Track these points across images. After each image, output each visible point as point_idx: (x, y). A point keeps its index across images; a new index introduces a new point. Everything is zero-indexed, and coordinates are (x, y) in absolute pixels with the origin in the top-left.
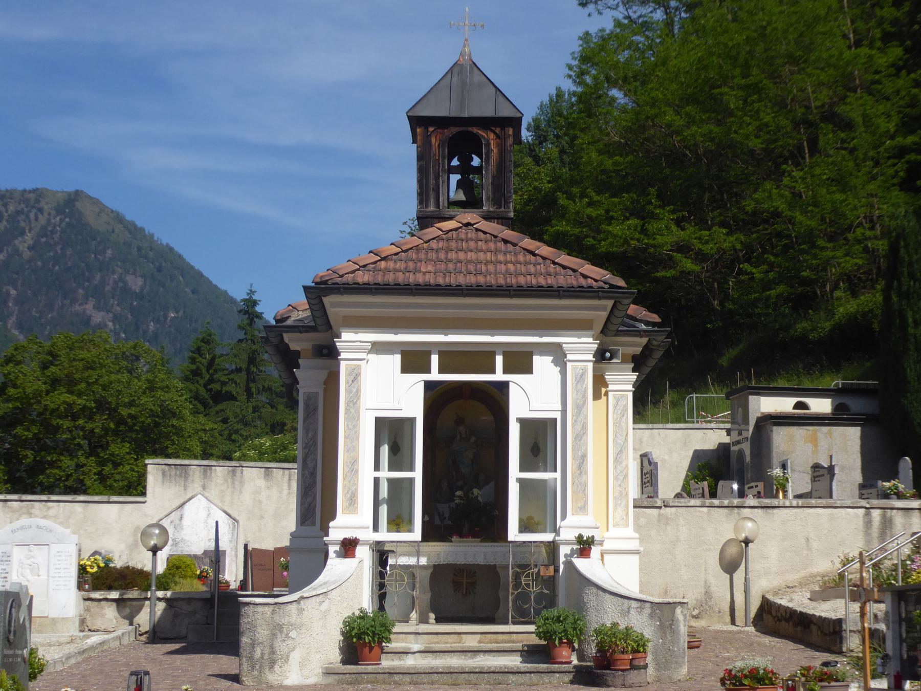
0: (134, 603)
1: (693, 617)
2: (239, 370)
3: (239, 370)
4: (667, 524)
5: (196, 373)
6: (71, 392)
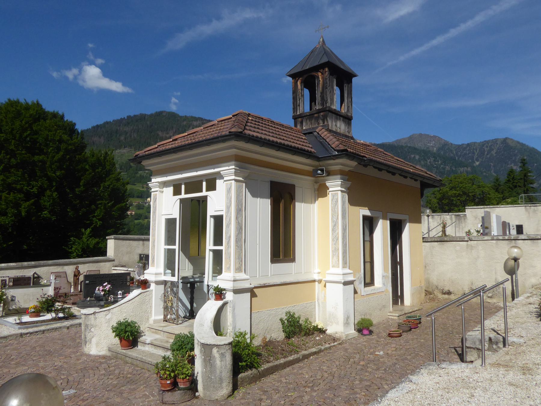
1: (489, 297)
2: (521, 179)
3: (521, 179)
4: (472, 249)
5: (509, 181)
6: (455, 190)
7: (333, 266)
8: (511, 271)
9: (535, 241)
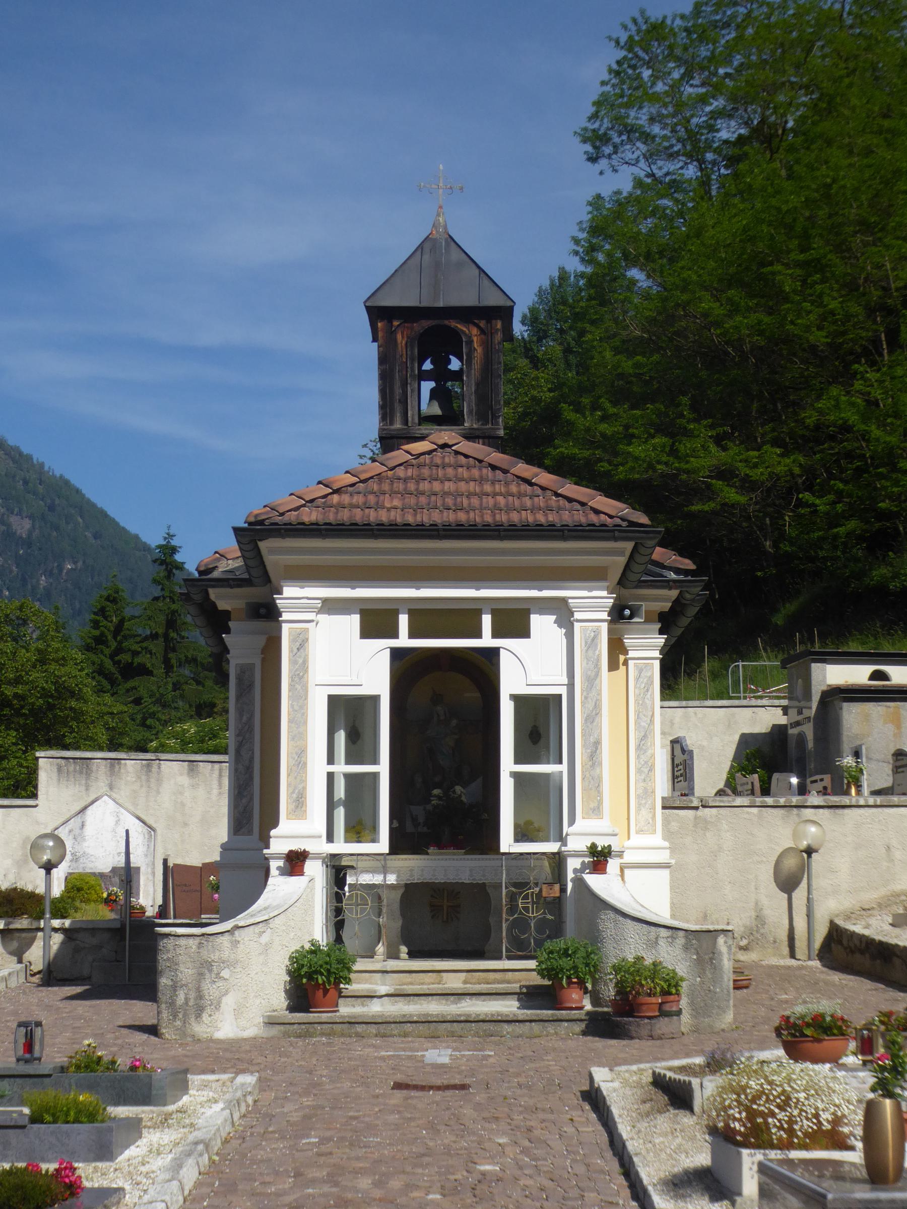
0: (24, 935)
1: (741, 948)
4: (706, 829)
5: (100, 640)
7: (640, 831)
8: (787, 883)
9: (840, 811)
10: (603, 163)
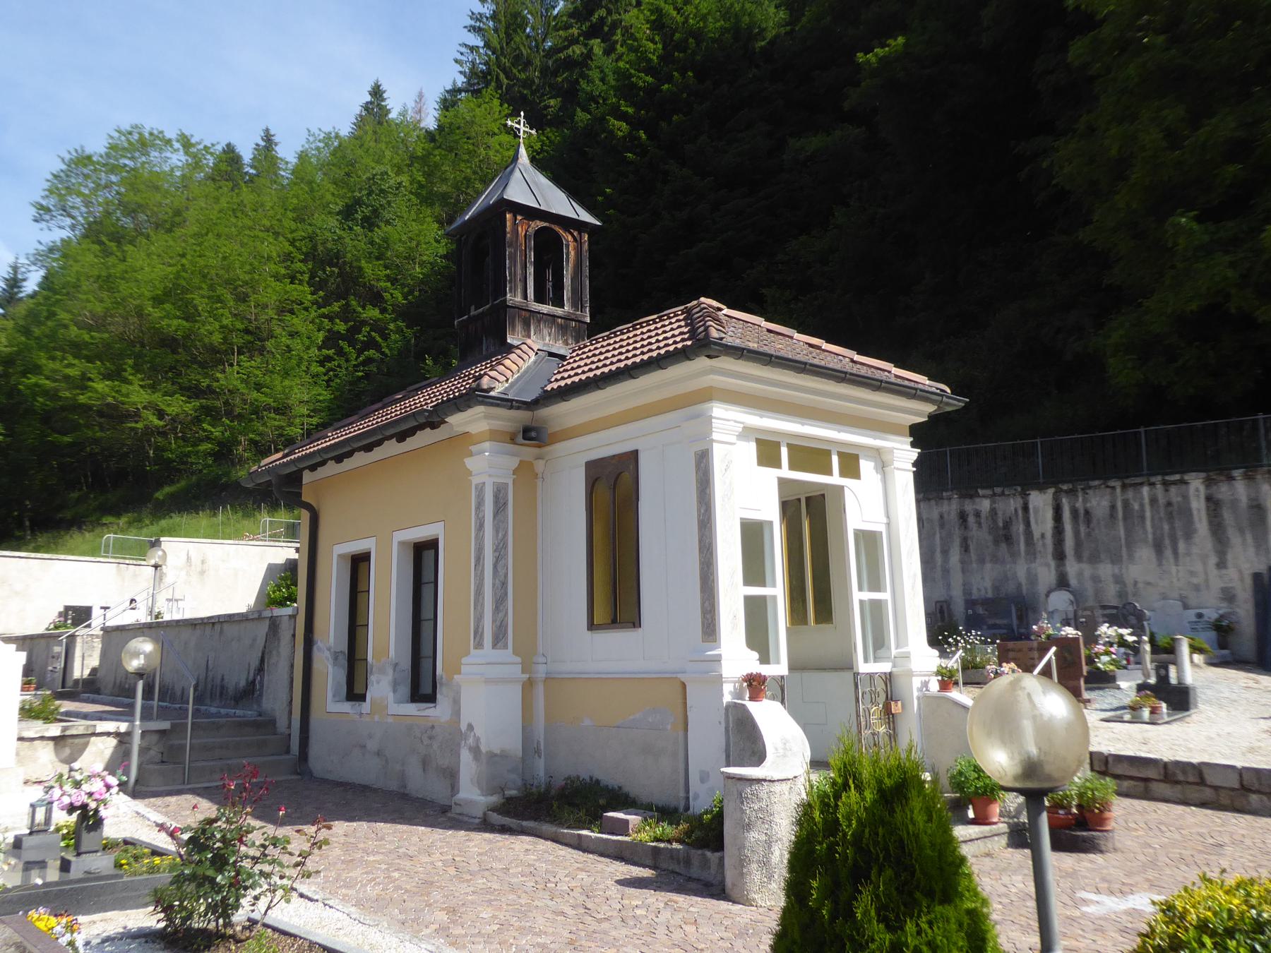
0: (77, 741)
10: (43, 225)
